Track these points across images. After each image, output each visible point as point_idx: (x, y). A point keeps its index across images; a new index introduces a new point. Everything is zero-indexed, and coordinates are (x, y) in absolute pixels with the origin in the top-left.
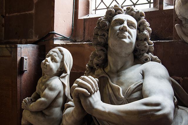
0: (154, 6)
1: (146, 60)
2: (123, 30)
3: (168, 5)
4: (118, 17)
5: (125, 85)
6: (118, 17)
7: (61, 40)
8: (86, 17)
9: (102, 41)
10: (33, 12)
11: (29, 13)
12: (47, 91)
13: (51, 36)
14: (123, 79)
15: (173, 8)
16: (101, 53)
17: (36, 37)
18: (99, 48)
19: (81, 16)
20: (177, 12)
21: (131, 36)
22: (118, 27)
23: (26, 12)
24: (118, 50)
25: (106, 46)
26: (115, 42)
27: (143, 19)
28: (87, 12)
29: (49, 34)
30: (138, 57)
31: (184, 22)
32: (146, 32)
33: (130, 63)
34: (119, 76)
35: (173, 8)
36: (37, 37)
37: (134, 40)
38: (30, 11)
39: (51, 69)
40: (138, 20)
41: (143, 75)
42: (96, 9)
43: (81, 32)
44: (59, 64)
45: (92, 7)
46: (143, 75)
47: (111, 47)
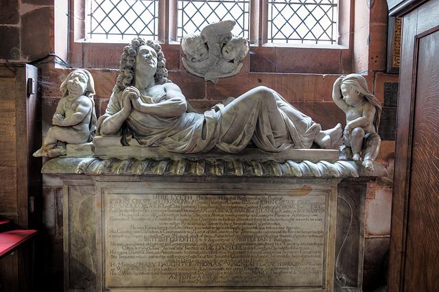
0: (159, 39)
1: (164, 82)
2: (149, 58)
3: (173, 40)
4: (143, 47)
5: (154, 96)
6: (143, 47)
7: (60, 64)
8: (82, 41)
9: (131, 65)
10: (19, 25)
11: (11, 27)
12: (80, 106)
13: (50, 59)
14: (151, 93)
15: (394, 151)
16: (131, 75)
17: (25, 58)
18: (129, 71)
19: (77, 39)
20: (184, 49)
21: (154, 63)
22: (145, 56)
23: (5, 25)
24: (146, 73)
25: (133, 69)
26: (145, 67)
27: (160, 51)
28: (83, 36)
29: (49, 56)
30: (158, 80)
31: (187, 57)
32: (163, 61)
33: (154, 83)
34: (147, 91)
35: (394, 151)
36: (28, 58)
37: (156, 65)
38: (13, 23)
39: (81, 88)
40: (157, 51)
41: (165, 90)
42: (91, 33)
43: (78, 57)
44: (86, 84)
45: (87, 30)
46: (165, 90)
47: (139, 70)
